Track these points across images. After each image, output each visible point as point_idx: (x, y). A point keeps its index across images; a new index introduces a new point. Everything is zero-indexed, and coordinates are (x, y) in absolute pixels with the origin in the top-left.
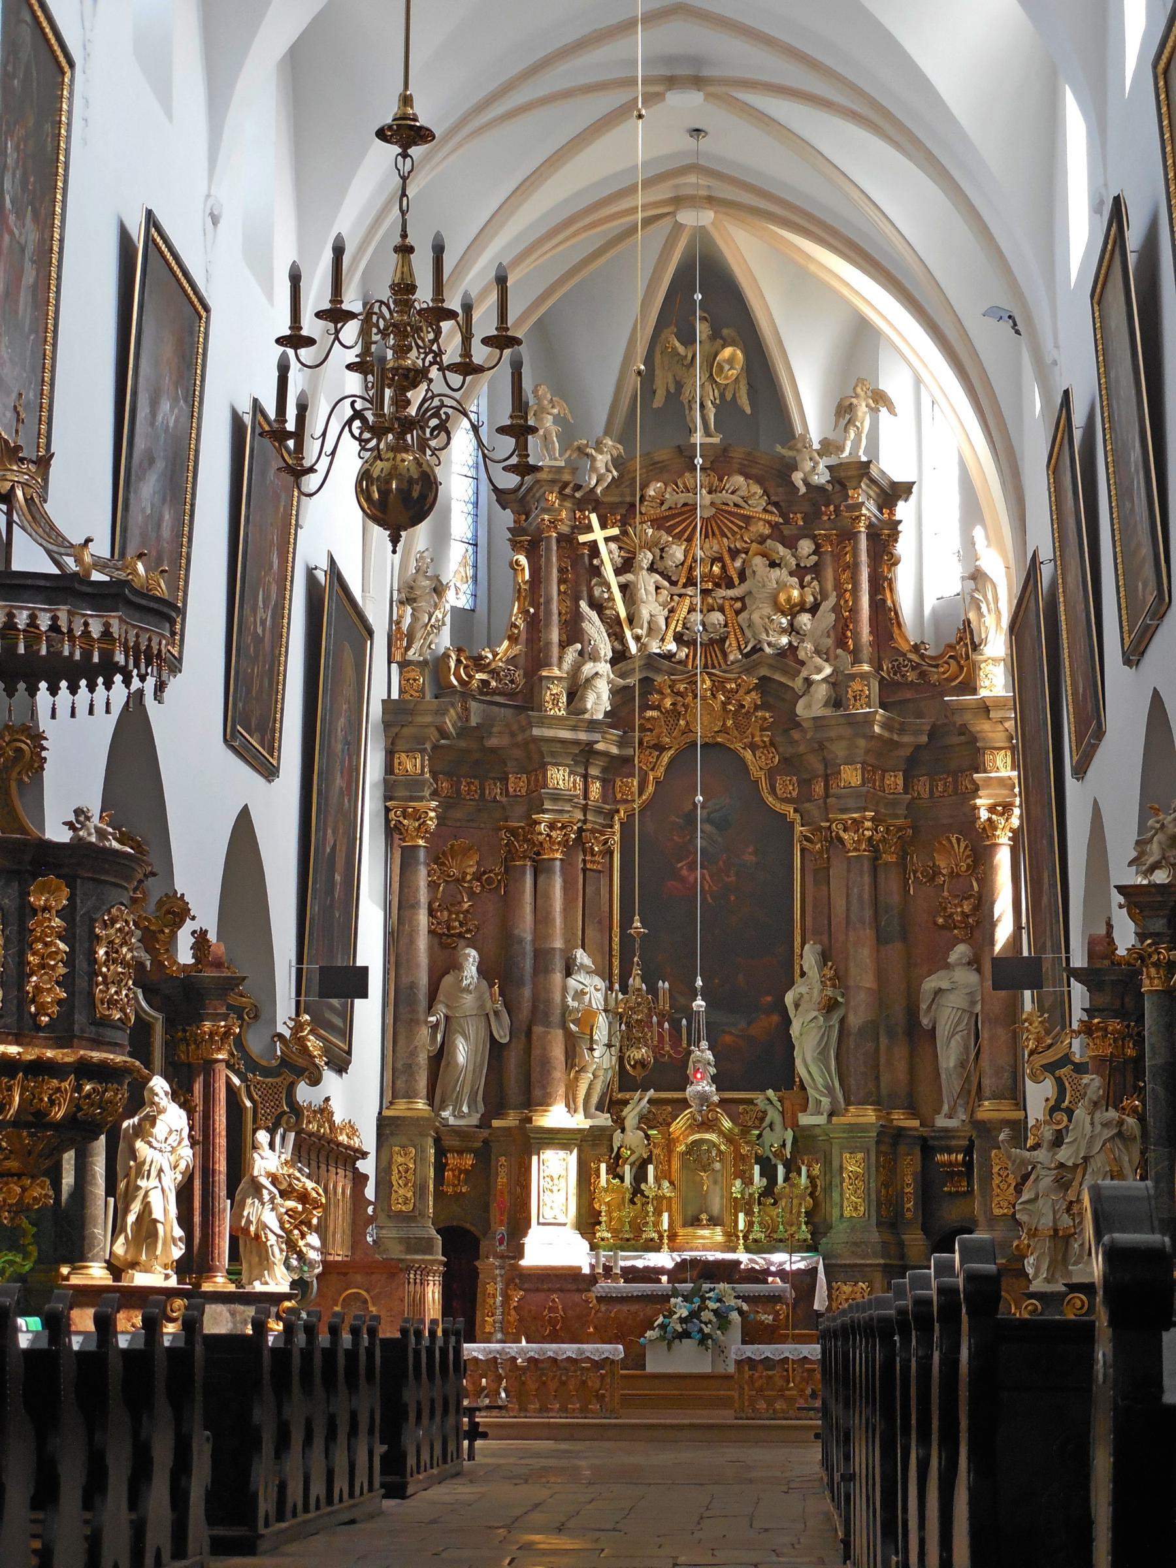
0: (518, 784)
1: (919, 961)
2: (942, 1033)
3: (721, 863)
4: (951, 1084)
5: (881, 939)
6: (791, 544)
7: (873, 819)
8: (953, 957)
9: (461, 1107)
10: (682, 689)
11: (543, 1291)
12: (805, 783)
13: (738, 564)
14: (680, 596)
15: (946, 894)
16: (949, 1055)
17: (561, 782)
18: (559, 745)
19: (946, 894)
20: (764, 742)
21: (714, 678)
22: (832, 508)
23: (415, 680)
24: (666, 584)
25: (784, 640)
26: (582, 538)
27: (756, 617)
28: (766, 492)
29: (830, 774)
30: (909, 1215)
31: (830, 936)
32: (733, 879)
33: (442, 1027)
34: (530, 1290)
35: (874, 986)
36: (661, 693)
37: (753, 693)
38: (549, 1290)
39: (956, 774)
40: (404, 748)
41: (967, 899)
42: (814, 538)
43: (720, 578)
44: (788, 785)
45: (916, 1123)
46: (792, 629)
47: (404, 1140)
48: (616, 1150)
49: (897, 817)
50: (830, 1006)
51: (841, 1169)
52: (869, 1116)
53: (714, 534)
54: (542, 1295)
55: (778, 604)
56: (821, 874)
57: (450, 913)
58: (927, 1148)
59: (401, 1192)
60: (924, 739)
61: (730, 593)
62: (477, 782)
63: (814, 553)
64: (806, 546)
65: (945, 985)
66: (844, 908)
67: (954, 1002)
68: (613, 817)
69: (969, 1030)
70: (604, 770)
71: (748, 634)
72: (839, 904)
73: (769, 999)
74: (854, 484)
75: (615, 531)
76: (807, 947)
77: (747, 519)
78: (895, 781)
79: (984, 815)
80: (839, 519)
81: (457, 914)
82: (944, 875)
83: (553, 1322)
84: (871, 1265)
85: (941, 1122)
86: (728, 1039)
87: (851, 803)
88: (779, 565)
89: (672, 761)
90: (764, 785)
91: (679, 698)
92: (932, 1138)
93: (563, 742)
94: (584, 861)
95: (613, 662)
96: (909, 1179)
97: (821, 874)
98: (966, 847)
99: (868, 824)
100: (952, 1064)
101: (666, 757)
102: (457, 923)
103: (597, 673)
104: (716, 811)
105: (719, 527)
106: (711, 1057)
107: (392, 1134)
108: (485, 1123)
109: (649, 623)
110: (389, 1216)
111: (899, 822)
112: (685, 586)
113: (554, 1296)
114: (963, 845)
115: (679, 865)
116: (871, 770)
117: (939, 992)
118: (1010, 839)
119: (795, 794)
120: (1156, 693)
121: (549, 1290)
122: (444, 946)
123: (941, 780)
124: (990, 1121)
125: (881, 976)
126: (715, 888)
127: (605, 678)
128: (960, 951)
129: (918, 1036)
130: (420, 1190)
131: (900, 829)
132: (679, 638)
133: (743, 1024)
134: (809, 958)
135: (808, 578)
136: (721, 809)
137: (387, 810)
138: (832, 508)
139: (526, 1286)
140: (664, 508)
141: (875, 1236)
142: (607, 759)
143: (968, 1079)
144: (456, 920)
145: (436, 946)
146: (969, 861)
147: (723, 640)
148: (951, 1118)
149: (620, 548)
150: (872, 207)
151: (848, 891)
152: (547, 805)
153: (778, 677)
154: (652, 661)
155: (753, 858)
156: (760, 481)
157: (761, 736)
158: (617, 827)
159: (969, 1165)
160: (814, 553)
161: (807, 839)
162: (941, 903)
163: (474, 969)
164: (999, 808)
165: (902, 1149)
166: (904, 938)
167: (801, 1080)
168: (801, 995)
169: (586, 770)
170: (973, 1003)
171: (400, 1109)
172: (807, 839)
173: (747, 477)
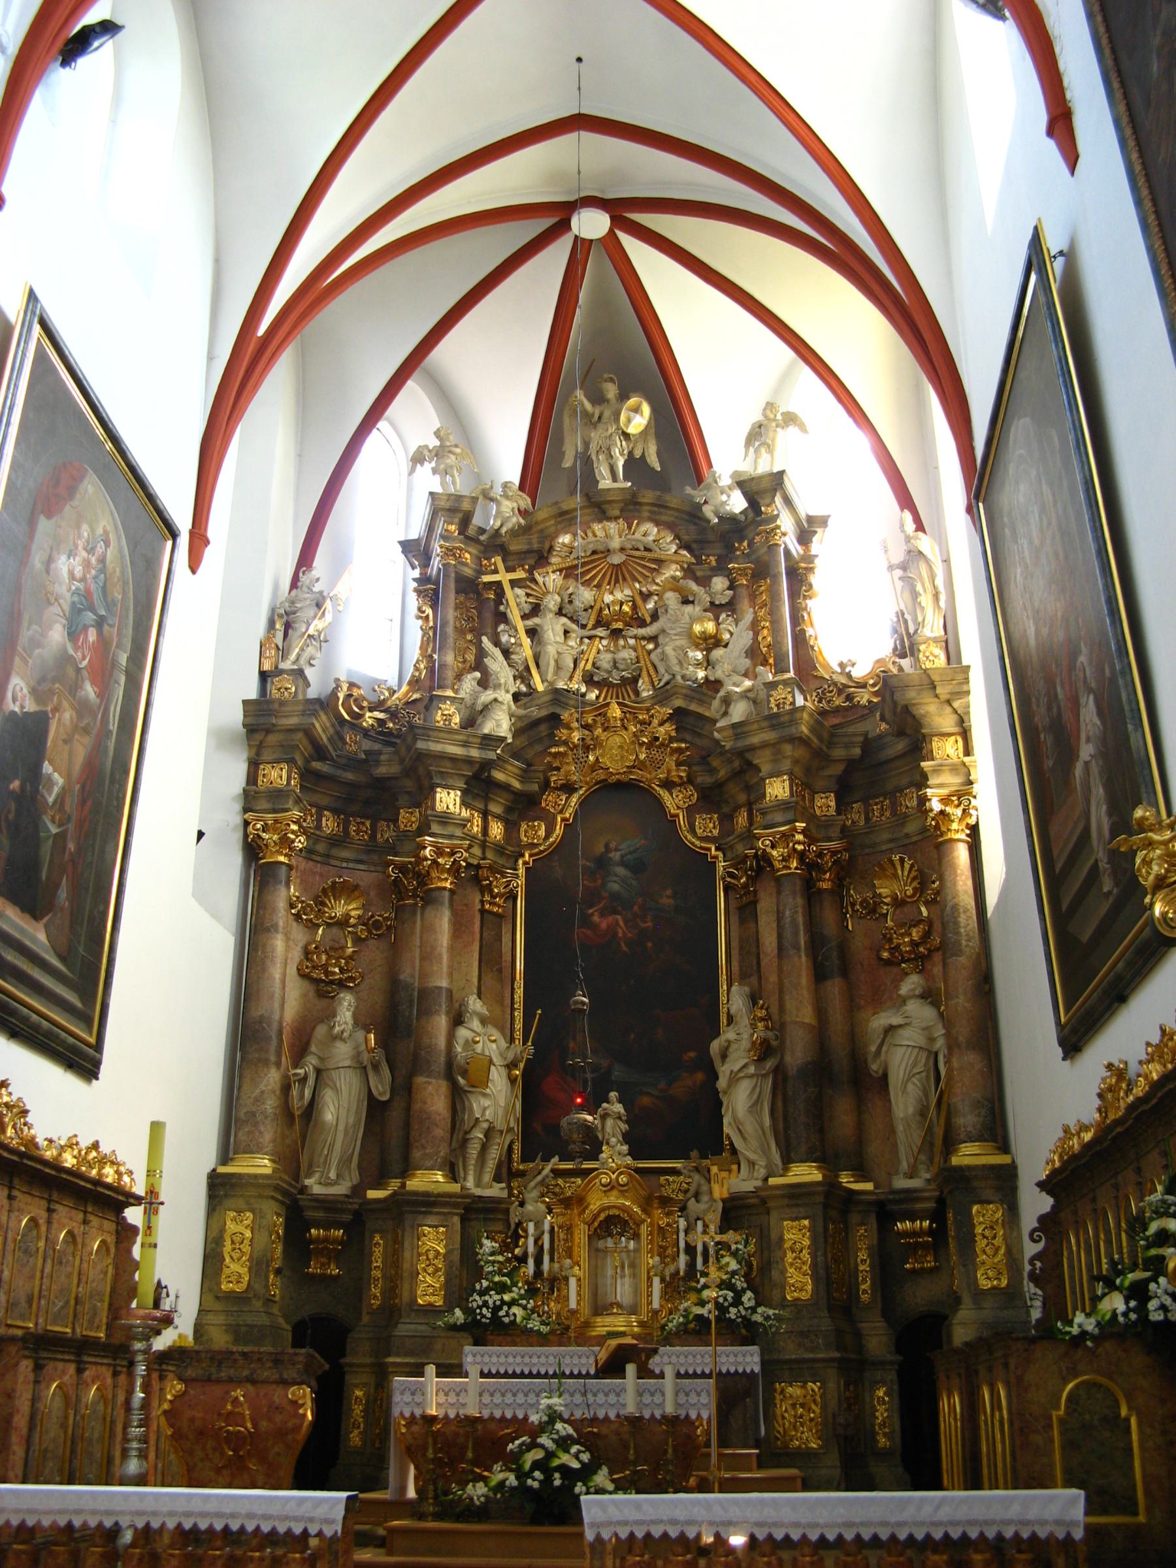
0: (408, 818)
1: (862, 1003)
2: (896, 1077)
3: (636, 908)
4: (908, 1137)
5: (820, 975)
6: (704, 582)
7: (803, 832)
8: (904, 989)
9: (328, 1172)
10: (590, 721)
11: (219, 1381)
12: (727, 819)
13: (650, 605)
14: (590, 638)
15: (890, 923)
16: (905, 1101)
17: (451, 806)
18: (448, 764)
19: (890, 923)
20: (681, 777)
21: (626, 709)
22: (745, 544)
23: (286, 689)
24: (574, 626)
25: (701, 674)
26: (487, 578)
27: (669, 650)
28: (677, 537)
29: (755, 792)
30: (865, 1298)
31: (760, 978)
32: (650, 924)
33: (311, 1081)
34: (194, 1380)
35: (814, 1022)
36: (570, 728)
37: (667, 725)
38: (230, 1380)
39: (894, 795)
40: (270, 758)
41: (915, 926)
42: (728, 574)
43: (631, 618)
44: (707, 825)
45: (869, 1186)
46: (708, 663)
47: (241, 1203)
48: (513, 1226)
49: (829, 840)
50: (764, 1051)
51: (781, 1239)
52: (806, 1173)
53: (624, 579)
54: (217, 1390)
55: (697, 642)
56: (746, 910)
57: (329, 957)
58: (885, 1210)
59: (235, 1267)
60: (857, 751)
61: (642, 632)
62: (368, 823)
63: (729, 588)
64: (719, 583)
65: (896, 1021)
66: (775, 944)
67: (910, 1037)
68: (516, 861)
69: (928, 1071)
70: (509, 810)
71: (662, 670)
72: (769, 941)
73: (692, 1054)
74: (767, 501)
75: (520, 574)
76: (734, 988)
77: (660, 562)
78: (825, 804)
79: (936, 806)
80: (749, 556)
81: (338, 959)
82: (887, 904)
83: (236, 1441)
84: (823, 1360)
85: (901, 1183)
86: (645, 1101)
87: (779, 818)
88: (693, 602)
89: (583, 803)
90: (682, 820)
91: (587, 732)
92: (890, 1201)
93: (453, 759)
94: (482, 902)
95: (516, 697)
96: (863, 1255)
97: (746, 910)
98: (912, 866)
99: (799, 837)
100: (911, 1110)
101: (574, 799)
102: (337, 970)
103: (496, 700)
104: (630, 853)
105: (629, 571)
106: (622, 1111)
107: (226, 1196)
108: (357, 1191)
109: (556, 661)
110: (217, 1298)
111: (832, 845)
112: (595, 627)
113: (239, 1393)
114: (907, 866)
115: (591, 911)
116: (805, 784)
117: (890, 1029)
118: (967, 835)
119: (716, 832)
120: (1072, 173)
121: (230, 1380)
122: (321, 995)
123: (876, 804)
124: (969, 1167)
125: (821, 1012)
126: (630, 935)
127: (505, 707)
128: (911, 983)
129: (869, 1084)
130: (258, 1266)
131: (834, 853)
132: (589, 680)
133: (662, 1085)
134: (734, 999)
135: (723, 616)
136: (634, 852)
137: (246, 823)
138: (745, 544)
139: (190, 1373)
140: (572, 556)
141: (825, 1323)
142: (511, 797)
143: (930, 1131)
144: (335, 965)
145: (312, 994)
146: (915, 884)
147: (635, 680)
148: (911, 1178)
149: (528, 595)
150: (778, 100)
151: (778, 915)
152: (435, 828)
153: (693, 707)
154: (558, 696)
155: (671, 901)
156: (670, 527)
157: (678, 770)
158: (521, 871)
159: (939, 1234)
160: (729, 588)
161: (731, 875)
162: (884, 936)
163: (349, 1015)
164: (954, 798)
165: (855, 1218)
166: (845, 972)
167: (731, 1144)
168: (729, 1042)
169: (486, 806)
170: (932, 1040)
171: (242, 1166)
172: (731, 875)
173: (657, 523)
